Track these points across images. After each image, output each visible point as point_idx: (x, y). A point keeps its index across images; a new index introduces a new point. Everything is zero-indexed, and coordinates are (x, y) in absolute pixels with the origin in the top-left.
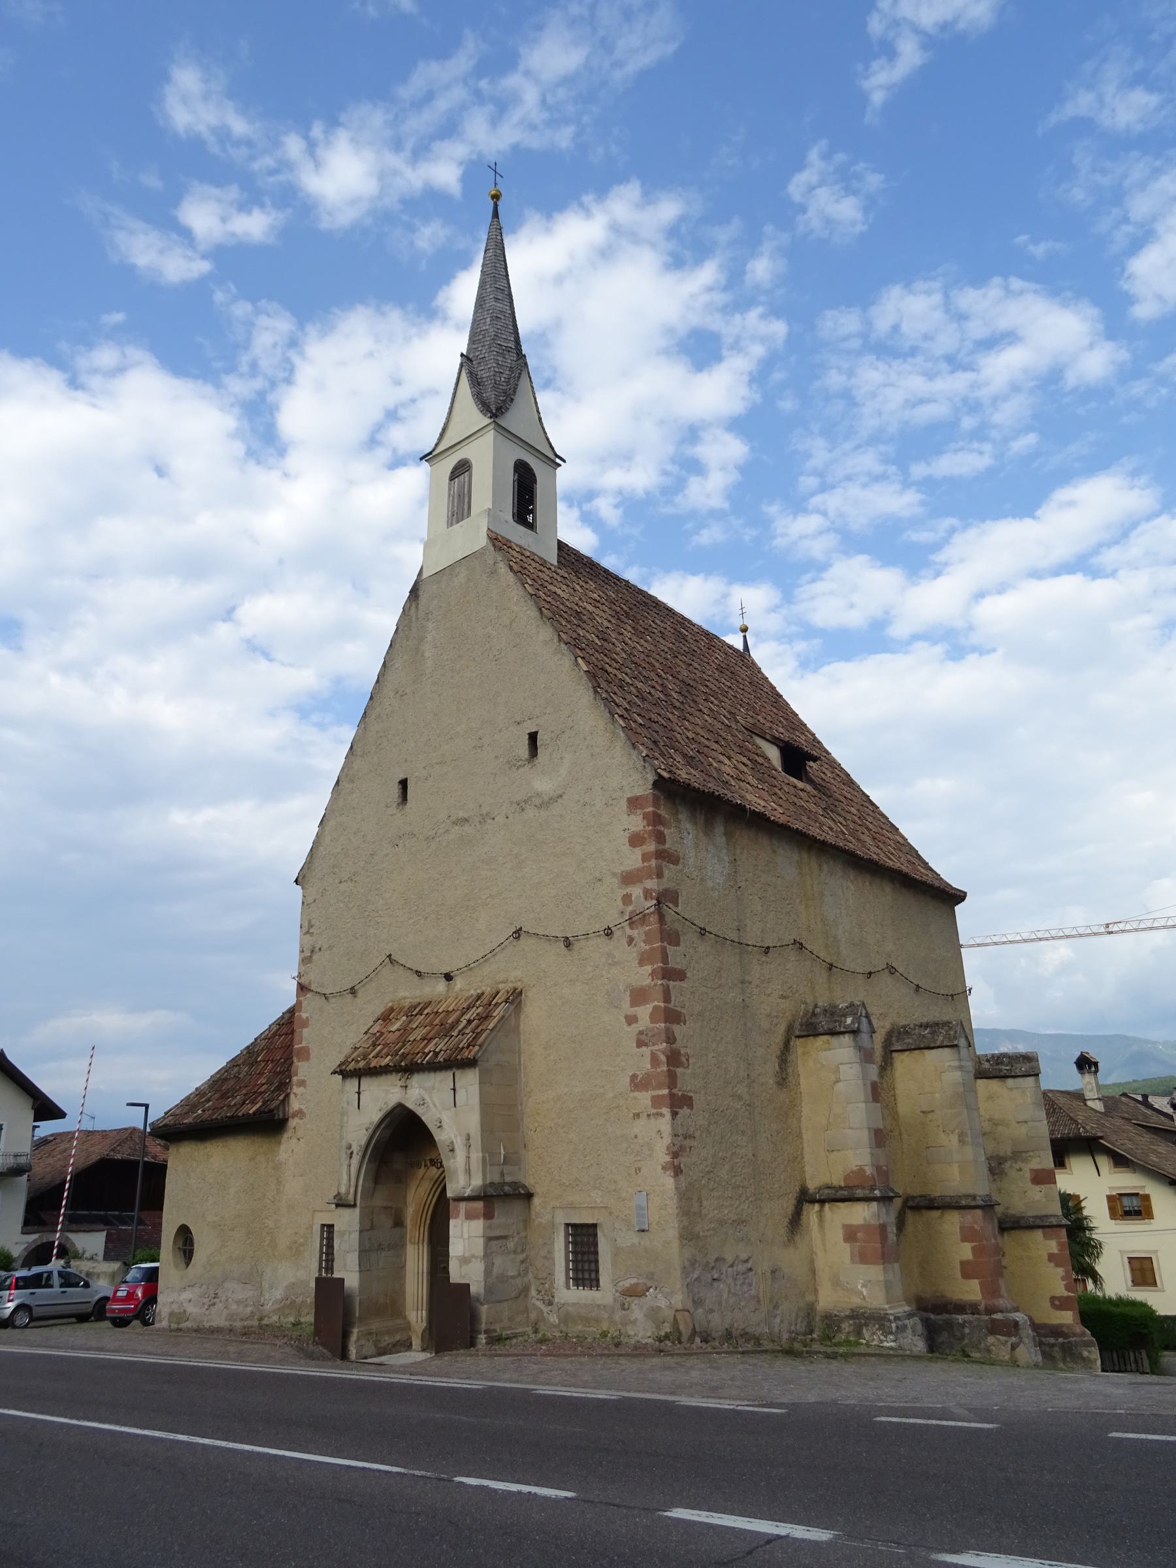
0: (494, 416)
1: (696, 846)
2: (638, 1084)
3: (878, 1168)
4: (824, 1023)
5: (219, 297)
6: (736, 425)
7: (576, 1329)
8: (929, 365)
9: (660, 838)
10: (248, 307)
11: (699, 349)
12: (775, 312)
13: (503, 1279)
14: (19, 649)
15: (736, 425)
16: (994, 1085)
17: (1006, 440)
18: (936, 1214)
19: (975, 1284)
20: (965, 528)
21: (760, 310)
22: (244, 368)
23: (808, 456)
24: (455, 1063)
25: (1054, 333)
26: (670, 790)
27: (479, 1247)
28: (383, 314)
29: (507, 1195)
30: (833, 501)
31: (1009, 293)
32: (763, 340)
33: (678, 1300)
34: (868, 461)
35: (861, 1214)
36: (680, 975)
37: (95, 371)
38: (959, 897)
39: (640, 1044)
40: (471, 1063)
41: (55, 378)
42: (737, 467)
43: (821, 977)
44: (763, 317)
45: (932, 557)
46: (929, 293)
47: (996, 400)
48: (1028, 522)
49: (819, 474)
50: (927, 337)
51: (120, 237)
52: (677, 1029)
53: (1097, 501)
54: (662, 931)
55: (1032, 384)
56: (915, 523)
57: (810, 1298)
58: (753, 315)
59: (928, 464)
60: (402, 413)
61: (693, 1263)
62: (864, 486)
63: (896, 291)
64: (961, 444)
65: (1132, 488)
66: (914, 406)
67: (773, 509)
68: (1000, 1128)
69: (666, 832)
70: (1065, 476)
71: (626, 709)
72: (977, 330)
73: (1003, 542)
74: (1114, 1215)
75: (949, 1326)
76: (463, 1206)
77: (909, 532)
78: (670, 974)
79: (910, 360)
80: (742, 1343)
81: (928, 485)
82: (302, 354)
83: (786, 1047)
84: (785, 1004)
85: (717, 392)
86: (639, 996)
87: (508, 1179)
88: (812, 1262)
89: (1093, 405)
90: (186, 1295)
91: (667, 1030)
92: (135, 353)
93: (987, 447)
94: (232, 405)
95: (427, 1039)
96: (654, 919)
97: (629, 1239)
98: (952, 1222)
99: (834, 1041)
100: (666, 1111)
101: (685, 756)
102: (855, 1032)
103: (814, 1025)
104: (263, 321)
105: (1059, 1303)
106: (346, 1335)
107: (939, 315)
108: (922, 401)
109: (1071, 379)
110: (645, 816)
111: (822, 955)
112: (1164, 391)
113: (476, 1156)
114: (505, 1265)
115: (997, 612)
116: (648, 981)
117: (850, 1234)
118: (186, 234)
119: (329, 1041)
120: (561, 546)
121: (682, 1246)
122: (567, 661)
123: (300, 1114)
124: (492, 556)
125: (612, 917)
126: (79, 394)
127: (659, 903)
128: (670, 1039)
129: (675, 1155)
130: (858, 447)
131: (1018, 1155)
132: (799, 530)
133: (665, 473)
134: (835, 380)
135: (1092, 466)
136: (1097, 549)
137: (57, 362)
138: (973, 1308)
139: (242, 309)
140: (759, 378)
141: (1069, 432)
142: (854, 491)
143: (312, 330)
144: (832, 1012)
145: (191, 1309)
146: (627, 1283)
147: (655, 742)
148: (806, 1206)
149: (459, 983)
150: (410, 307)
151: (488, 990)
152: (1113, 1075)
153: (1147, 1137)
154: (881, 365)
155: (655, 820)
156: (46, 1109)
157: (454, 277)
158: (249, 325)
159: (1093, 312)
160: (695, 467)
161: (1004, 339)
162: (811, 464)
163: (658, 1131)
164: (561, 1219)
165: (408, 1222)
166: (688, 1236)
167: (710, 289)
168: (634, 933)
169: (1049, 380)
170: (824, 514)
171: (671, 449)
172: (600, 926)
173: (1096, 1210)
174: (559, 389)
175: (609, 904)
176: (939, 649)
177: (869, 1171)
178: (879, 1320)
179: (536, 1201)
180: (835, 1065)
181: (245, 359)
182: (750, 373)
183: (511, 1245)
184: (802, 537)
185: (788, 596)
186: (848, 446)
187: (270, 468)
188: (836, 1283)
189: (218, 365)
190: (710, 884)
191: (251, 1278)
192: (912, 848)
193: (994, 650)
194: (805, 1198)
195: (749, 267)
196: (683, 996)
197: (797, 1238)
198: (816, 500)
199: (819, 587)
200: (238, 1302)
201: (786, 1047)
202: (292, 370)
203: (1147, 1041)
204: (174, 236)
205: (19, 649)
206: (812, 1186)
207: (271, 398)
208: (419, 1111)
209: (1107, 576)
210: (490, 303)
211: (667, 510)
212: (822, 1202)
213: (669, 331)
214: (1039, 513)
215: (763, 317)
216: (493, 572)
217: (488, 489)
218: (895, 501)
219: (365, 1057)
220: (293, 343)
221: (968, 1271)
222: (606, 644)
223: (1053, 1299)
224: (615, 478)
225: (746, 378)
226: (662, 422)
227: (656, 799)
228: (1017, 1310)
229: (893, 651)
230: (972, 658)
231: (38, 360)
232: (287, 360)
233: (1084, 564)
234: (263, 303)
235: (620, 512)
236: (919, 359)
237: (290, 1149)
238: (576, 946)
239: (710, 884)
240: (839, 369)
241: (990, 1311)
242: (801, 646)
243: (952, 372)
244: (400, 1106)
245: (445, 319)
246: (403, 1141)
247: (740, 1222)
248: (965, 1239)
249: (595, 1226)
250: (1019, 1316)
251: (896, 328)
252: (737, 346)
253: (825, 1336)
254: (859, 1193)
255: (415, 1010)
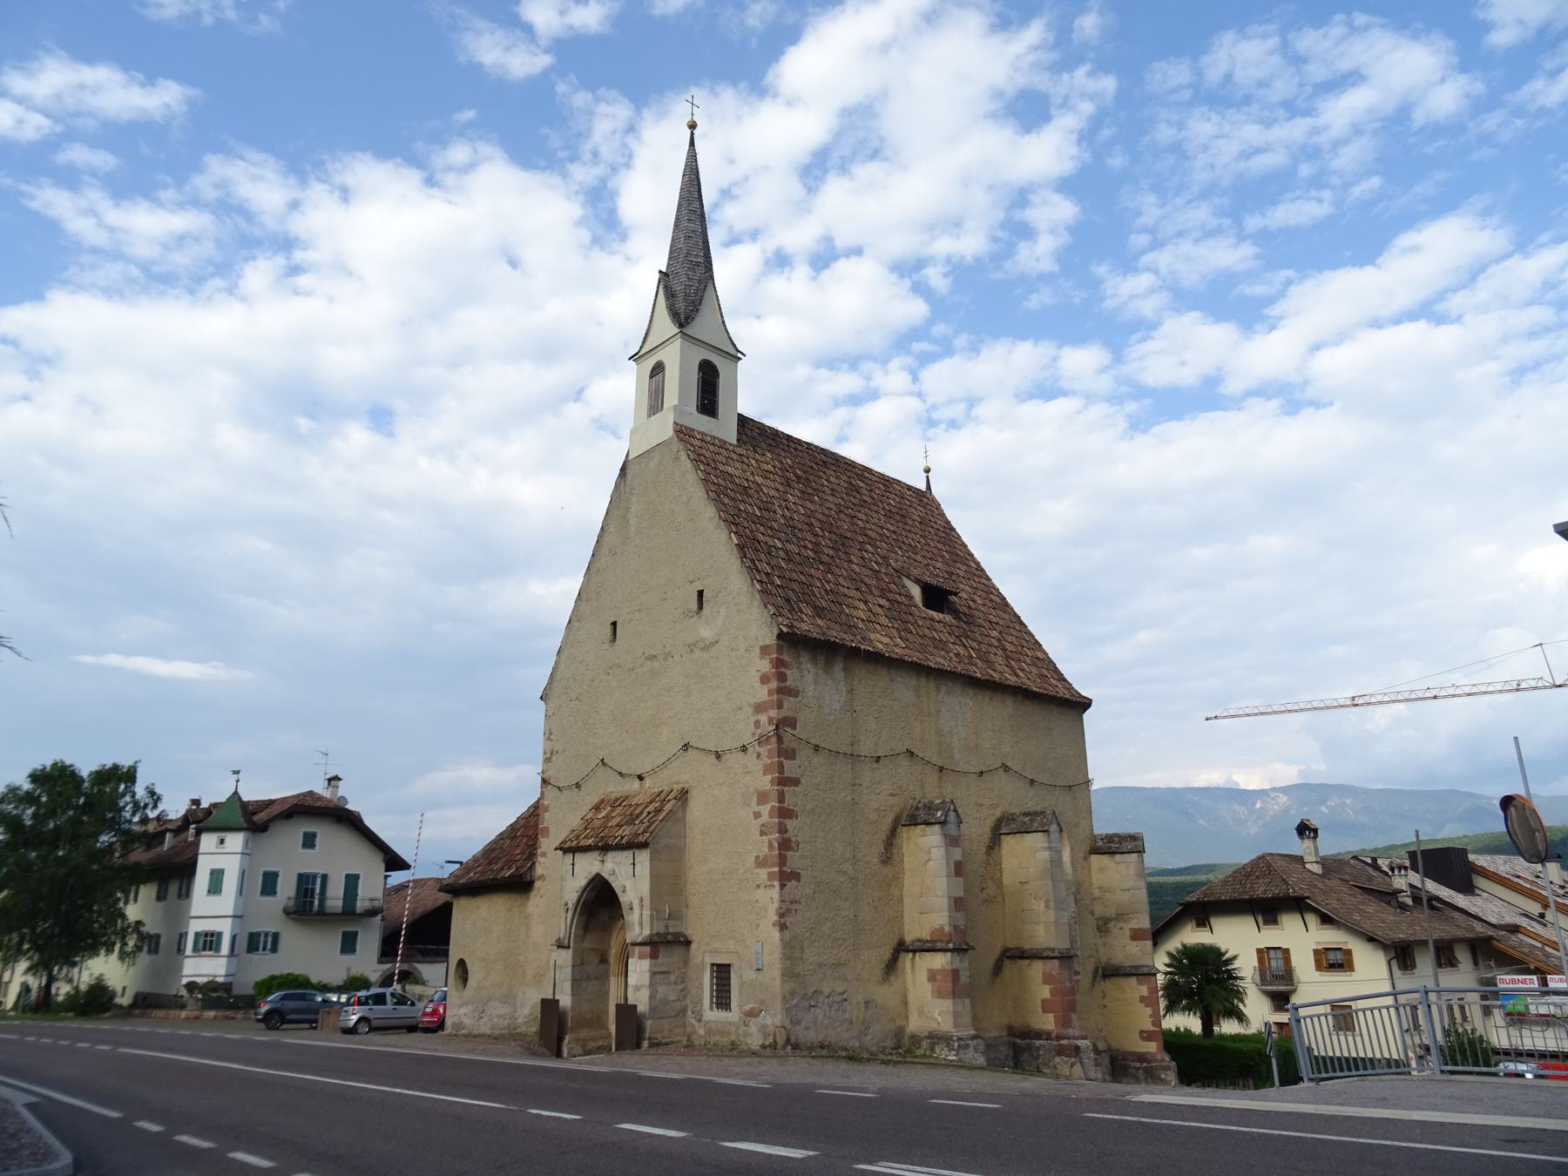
0: (681, 326)
1: (816, 682)
2: (760, 863)
3: (955, 927)
4: (922, 815)
5: (561, 88)
6: (1065, 186)
7: (715, 1039)
8: (1265, 113)
9: (782, 677)
10: (589, 96)
11: (1026, 110)
12: (1101, 68)
13: (665, 1002)
14: (391, 435)
15: (1065, 186)
16: (1105, 859)
17: (1347, 186)
18: (1026, 962)
19: (1051, 1017)
20: (1304, 278)
21: (1088, 66)
22: (587, 157)
23: (1138, 213)
24: (633, 845)
25: (1406, 69)
26: (791, 641)
27: (646, 979)
28: (716, 95)
29: (669, 942)
30: (1164, 259)
31: (1353, 29)
32: (1092, 97)
33: (778, 1020)
34: (1201, 214)
35: (940, 961)
36: (795, 782)
37: (450, 168)
38: (1085, 704)
39: (762, 833)
40: (644, 845)
41: (414, 177)
42: (1068, 228)
43: (932, 778)
44: (1090, 74)
45: (1266, 311)
46: (1264, 37)
47: (1337, 144)
48: (1369, 269)
49: (1150, 230)
50: (1262, 84)
51: (468, 38)
52: (790, 823)
53: (1444, 243)
54: (779, 749)
55: (1378, 124)
56: (1249, 276)
57: (900, 1022)
58: (1081, 72)
59: (1264, 215)
60: (735, 191)
61: (793, 993)
62: (1197, 241)
63: (1228, 37)
64: (1298, 193)
65: (1483, 229)
66: (1248, 158)
67: (1102, 270)
68: (1107, 895)
69: (788, 672)
70: (1410, 220)
71: (767, 574)
72: (1316, 72)
73: (1343, 291)
74: (1319, 967)
75: (1029, 1048)
76: (637, 949)
77: (1241, 287)
78: (784, 781)
79: (1245, 109)
80: (826, 1051)
81: (1263, 237)
82: (638, 138)
83: (893, 832)
84: (894, 800)
85: (1046, 153)
86: (762, 798)
87: (671, 930)
88: (905, 996)
89: (1442, 142)
90: (463, 1011)
91: (780, 824)
92: (486, 149)
93: (1327, 194)
94: (577, 193)
95: (619, 826)
96: (774, 740)
97: (750, 975)
98: (1037, 969)
99: (929, 829)
100: (776, 883)
101: (815, 608)
102: (943, 823)
103: (915, 817)
104: (602, 108)
105: (1147, 1036)
106: (560, 1040)
107: (1275, 60)
108: (1258, 151)
109: (1419, 118)
110: (771, 661)
111: (934, 760)
112: (1519, 123)
113: (647, 913)
114: (667, 992)
115: (1336, 363)
116: (769, 787)
117: (932, 976)
118: (528, 30)
119: (561, 823)
120: (743, 421)
121: (783, 982)
122: (724, 534)
123: (542, 877)
124: (677, 445)
125: (747, 738)
126: (435, 191)
127: (777, 727)
128: (782, 830)
129: (782, 916)
130: (1190, 202)
131: (1121, 916)
132: (1130, 290)
133: (994, 239)
134: (1164, 134)
135: (1441, 206)
136: (1442, 295)
137: (415, 161)
138: (1047, 1035)
139: (581, 99)
140: (1086, 137)
141: (1416, 170)
142: (1186, 247)
143: (648, 114)
144: (930, 807)
145: (466, 1021)
146: (747, 1007)
147: (788, 600)
148: (902, 955)
149: (648, 783)
150: (742, 86)
151: (666, 789)
152: (1331, 844)
153: (1361, 896)
154: (1215, 117)
155: (779, 663)
156: (394, 862)
157: (783, 53)
158: (591, 113)
159: (1450, 43)
160: (1025, 232)
161: (1354, 78)
162: (1141, 221)
163: (770, 898)
164: (709, 960)
165: (612, 960)
166: (789, 974)
167: (1036, 48)
168: (761, 750)
169: (1396, 123)
170: (1156, 272)
171: (1001, 215)
172: (739, 744)
173: (1303, 964)
174: (886, 159)
175: (746, 726)
176: (1274, 404)
177: (947, 929)
178: (946, 1039)
179: (693, 946)
180: (926, 851)
181: (587, 147)
182: (1081, 131)
183: (672, 978)
184: (1133, 297)
185: (1118, 357)
186: (1179, 201)
187: (613, 253)
188: (921, 1012)
189: (562, 154)
190: (827, 710)
191: (509, 999)
192: (1051, 661)
193: (1331, 404)
194: (901, 948)
195: (1077, 23)
196: (793, 797)
197: (892, 978)
198: (1147, 258)
199: (1150, 346)
200: (499, 1016)
201: (893, 832)
202: (630, 157)
203: (1483, 797)
204: (518, 32)
205: (391, 435)
206: (908, 939)
207: (610, 184)
208: (611, 880)
209: (1452, 322)
210: (685, 224)
211: (999, 275)
212: (914, 951)
213: (998, 94)
214: (1379, 261)
215: (1090, 74)
216: (677, 459)
217: (679, 386)
218: (1227, 255)
219: (577, 837)
220: (631, 129)
221: (1046, 1007)
222: (766, 514)
223: (1142, 1032)
224: (945, 246)
225: (1075, 137)
226: (991, 188)
227: (779, 649)
228: (1084, 1038)
229: (1225, 409)
230: (1308, 412)
231: (399, 160)
232: (625, 145)
233: (1429, 311)
234: (602, 91)
235: (949, 281)
236: (1254, 108)
237: (537, 903)
238: (724, 758)
239: (827, 710)
240: (1168, 121)
241: (1058, 1038)
242: (1132, 407)
243: (1290, 119)
244: (598, 875)
245: (775, 96)
246: (600, 903)
247: (838, 965)
248: (1046, 982)
249: (729, 965)
250: (1082, 1043)
251: (1228, 77)
252: (1065, 105)
253: (906, 1049)
254: (939, 945)
255: (617, 802)
